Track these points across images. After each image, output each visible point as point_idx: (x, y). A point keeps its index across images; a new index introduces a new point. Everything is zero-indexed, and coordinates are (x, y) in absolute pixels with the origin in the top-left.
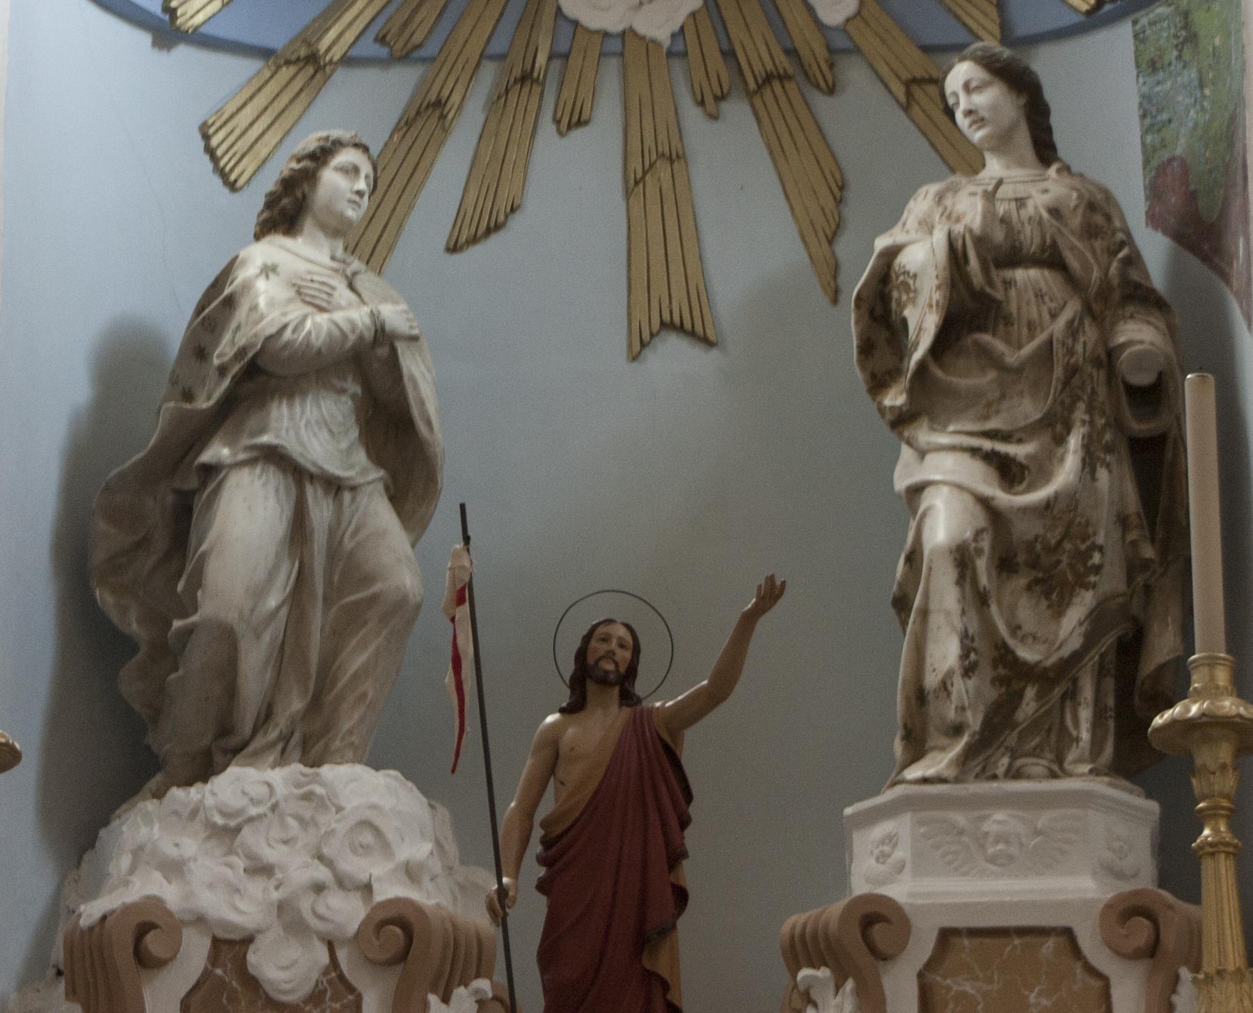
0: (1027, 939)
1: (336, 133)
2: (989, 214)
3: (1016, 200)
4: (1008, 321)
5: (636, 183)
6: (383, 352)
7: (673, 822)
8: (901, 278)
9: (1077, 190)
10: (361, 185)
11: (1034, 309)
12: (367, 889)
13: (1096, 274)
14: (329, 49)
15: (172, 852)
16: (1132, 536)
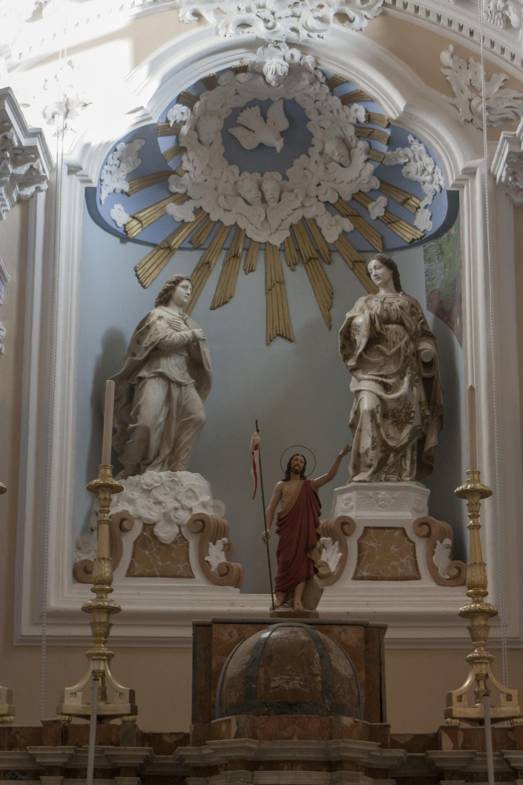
0: (391, 531)
1: (181, 275)
2: (382, 308)
3: (390, 303)
4: (387, 341)
5: (269, 290)
6: (195, 344)
7: (316, 515)
8: (355, 327)
9: (408, 301)
10: (189, 292)
11: (395, 337)
12: (191, 510)
13: (414, 328)
14: (174, 245)
15: (131, 497)
16: (423, 408)
